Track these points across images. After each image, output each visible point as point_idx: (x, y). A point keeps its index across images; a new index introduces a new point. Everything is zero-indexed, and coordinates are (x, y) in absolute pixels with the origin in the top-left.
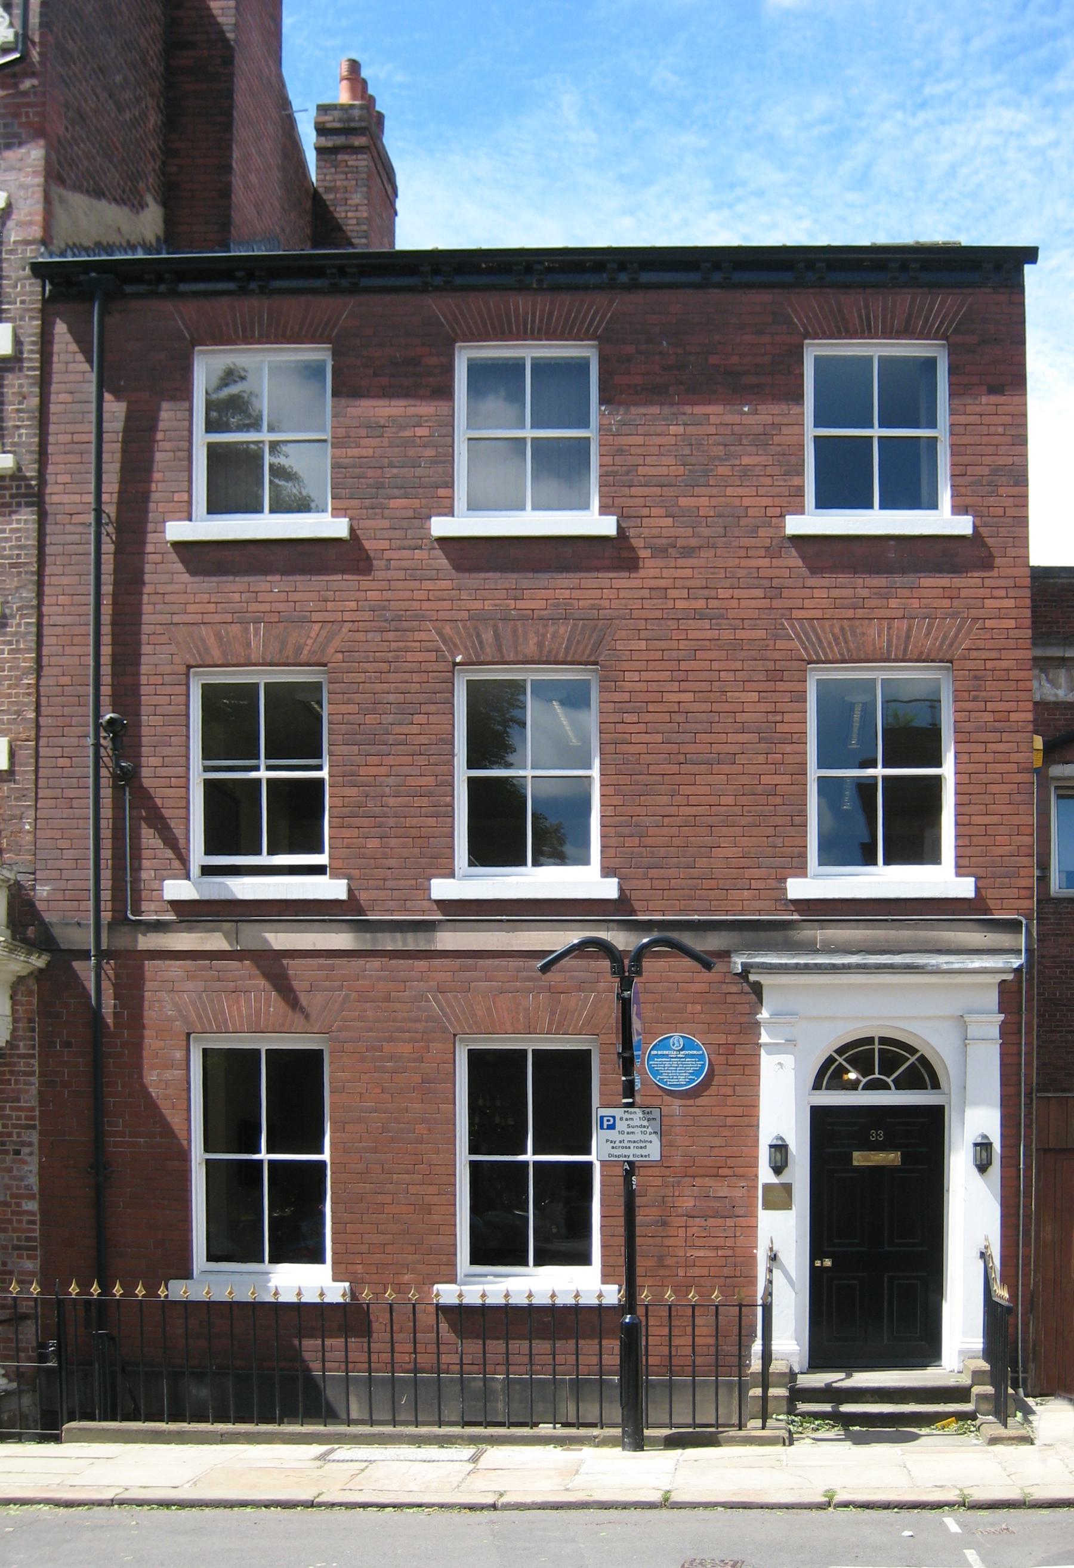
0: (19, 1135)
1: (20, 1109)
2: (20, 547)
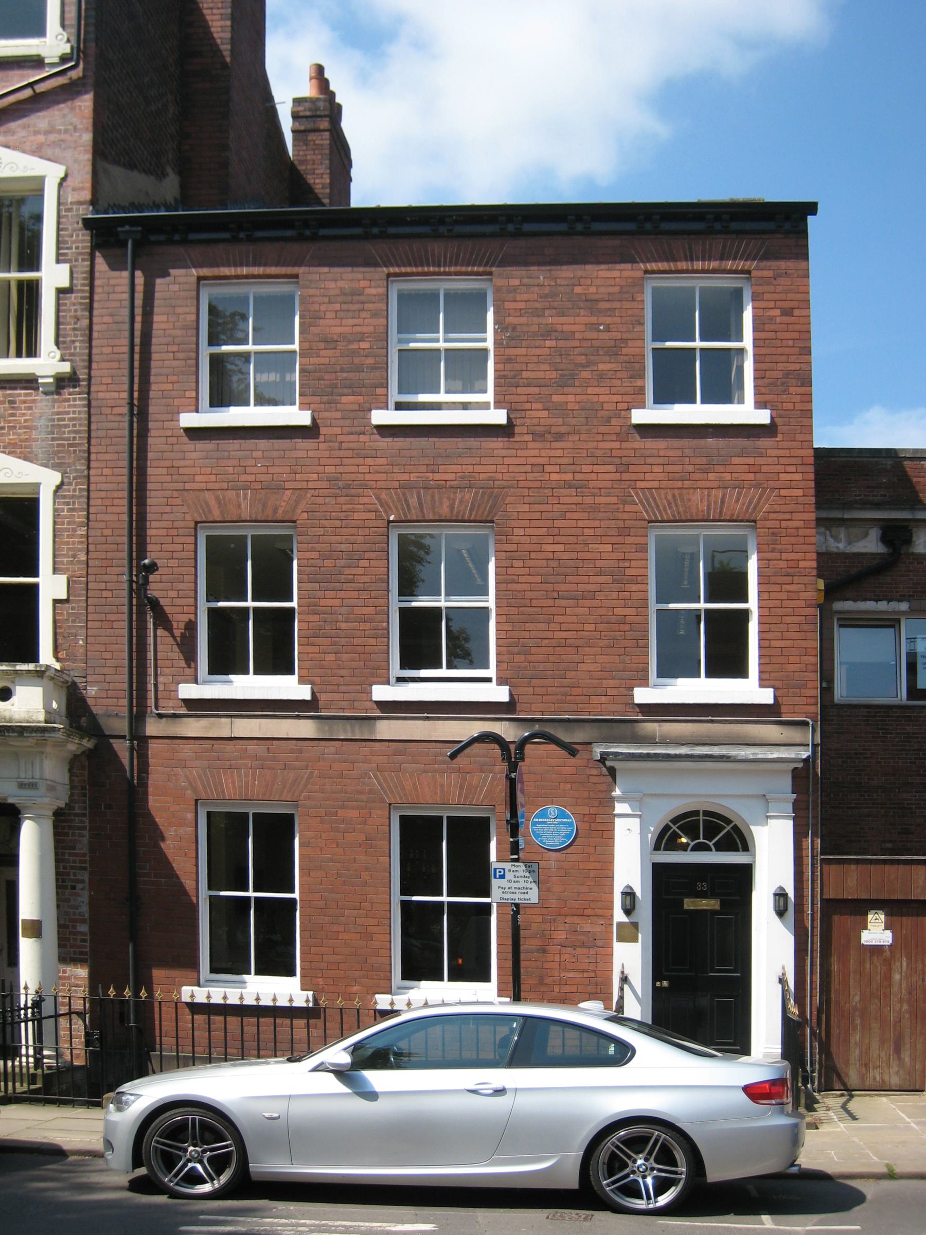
0: (75, 875)
1: (76, 855)
2: (75, 432)
